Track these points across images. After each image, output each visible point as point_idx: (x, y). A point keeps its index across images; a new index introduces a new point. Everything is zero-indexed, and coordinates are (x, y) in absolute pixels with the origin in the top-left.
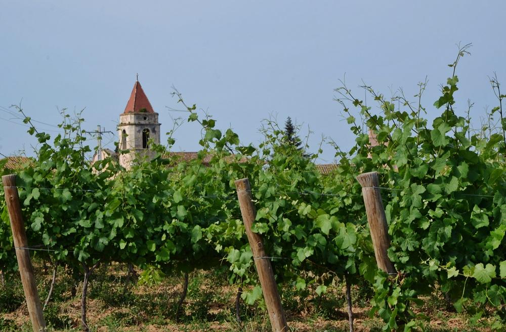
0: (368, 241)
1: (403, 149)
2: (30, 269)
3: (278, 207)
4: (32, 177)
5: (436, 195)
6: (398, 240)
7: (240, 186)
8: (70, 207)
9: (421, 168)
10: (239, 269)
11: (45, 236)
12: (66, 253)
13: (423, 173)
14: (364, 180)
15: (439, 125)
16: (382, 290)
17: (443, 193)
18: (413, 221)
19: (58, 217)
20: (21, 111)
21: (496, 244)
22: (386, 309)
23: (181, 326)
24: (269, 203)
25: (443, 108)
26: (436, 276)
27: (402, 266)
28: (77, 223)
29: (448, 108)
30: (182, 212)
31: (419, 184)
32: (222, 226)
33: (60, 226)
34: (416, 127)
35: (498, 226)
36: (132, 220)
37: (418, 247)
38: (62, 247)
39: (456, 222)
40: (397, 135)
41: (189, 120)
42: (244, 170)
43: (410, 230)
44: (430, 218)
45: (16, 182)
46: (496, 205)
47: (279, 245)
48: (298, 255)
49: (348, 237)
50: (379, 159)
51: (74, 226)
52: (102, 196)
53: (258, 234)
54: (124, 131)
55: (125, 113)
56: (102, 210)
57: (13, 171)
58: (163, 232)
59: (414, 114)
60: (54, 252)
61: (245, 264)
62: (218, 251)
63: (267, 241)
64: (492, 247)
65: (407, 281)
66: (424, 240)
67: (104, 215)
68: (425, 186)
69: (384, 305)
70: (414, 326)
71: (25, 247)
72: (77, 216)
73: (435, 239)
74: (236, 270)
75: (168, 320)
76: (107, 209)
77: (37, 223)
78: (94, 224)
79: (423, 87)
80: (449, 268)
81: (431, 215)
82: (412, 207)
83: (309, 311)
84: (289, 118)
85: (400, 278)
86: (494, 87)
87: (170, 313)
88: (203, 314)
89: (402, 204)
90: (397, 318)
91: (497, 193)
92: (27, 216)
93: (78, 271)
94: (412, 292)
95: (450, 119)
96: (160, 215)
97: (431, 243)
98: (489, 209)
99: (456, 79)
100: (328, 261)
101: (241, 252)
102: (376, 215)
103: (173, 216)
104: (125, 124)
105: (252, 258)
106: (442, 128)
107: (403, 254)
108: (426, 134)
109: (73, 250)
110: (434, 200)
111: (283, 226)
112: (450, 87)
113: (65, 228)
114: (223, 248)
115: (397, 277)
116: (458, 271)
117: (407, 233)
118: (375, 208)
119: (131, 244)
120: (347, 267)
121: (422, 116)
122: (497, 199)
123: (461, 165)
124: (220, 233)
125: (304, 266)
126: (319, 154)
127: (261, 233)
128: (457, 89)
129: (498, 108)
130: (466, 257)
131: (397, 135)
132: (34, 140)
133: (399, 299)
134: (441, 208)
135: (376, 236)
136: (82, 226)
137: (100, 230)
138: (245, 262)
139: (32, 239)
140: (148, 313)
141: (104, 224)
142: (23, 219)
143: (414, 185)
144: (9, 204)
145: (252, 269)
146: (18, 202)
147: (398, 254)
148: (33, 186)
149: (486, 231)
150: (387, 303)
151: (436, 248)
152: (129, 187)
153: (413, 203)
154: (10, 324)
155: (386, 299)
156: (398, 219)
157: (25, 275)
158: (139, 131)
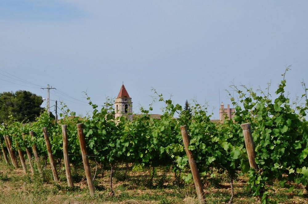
0: (245, 154)
1: (261, 113)
2: (88, 164)
3: (199, 139)
4: (89, 124)
5: (277, 134)
6: (260, 154)
7: (183, 129)
8: (105, 137)
9: (269, 121)
10: (181, 166)
11: (95, 150)
12: (104, 158)
13: (271, 124)
14: (244, 126)
15: (278, 102)
16: (252, 177)
17: (280, 133)
18: (267, 145)
19: (100, 142)
20: (86, 94)
21: (305, 156)
22: (254, 185)
23: (152, 190)
24: (196, 137)
25: (280, 94)
26: (277, 171)
27: (262, 166)
28: (108, 145)
29: (281, 94)
30: (155, 142)
31: (269, 129)
32: (173, 146)
33: (101, 146)
34: (267, 103)
35: (305, 148)
36: (132, 144)
37: (269, 157)
38: (102, 155)
39: (287, 146)
40: (258, 106)
41: (159, 100)
42: (184, 122)
43: (265, 150)
44: (274, 144)
45: (82, 127)
46: (304, 138)
47: (200, 156)
48: (209, 160)
49: (236, 152)
50: (245, 117)
51: (107, 146)
52: (119, 133)
53: (191, 150)
54: (117, 106)
55: (118, 98)
56: (119, 139)
57: (81, 122)
58: (146, 149)
59: (265, 97)
60: (98, 157)
61: (184, 164)
62: (172, 158)
63: (195, 154)
64: (303, 158)
65: (264, 173)
66: (272, 154)
67: (120, 141)
68: (272, 130)
69: (253, 184)
70: (268, 194)
71: (86, 155)
72: (108, 142)
73: (277, 154)
74: (180, 166)
75: (146, 188)
76: (122, 138)
77: (92, 144)
78: (116, 145)
79: (269, 85)
80: (290, 169)
81: (275, 143)
82: (266, 139)
83: (207, 184)
84: (187, 100)
85: (261, 172)
86: (303, 85)
87: (147, 185)
88: (161, 185)
89: (261, 138)
90: (260, 190)
91: (305, 133)
92: (87, 141)
93: (106, 166)
94: (267, 178)
95: (283, 99)
96: (144, 142)
97: (275, 156)
98: (301, 140)
99: (285, 81)
100: (223, 162)
101: (183, 158)
102: (250, 143)
103: (152, 143)
104: (118, 103)
105: (188, 161)
106: (279, 103)
107: (262, 161)
108: (271, 106)
109: (107, 157)
110: (276, 136)
111: (202, 147)
112: (282, 85)
113: (103, 147)
114: (175, 156)
115: (259, 171)
116: (294, 170)
117: (264, 151)
118: (249, 140)
119: (132, 154)
120: (231, 166)
121: (269, 98)
122: (305, 136)
123: (288, 120)
124: (172, 150)
125: (211, 165)
126: (212, 115)
127: (192, 150)
128: (286, 86)
129: (305, 95)
130: (291, 162)
131: (258, 106)
132: (91, 107)
133: (261, 181)
134: (280, 140)
135: (250, 152)
136: (111, 146)
137: (118, 148)
138: (184, 163)
139: (89, 152)
140: (137, 184)
141: (121, 145)
142: (85, 142)
143: (267, 129)
144: (79, 136)
145: (187, 166)
146: (83, 135)
147: (260, 160)
148: (90, 128)
149: (300, 151)
150: (255, 183)
151: (277, 158)
152: (131, 128)
153: (266, 137)
154: (78, 188)
155: (255, 181)
156: (260, 144)
157: (86, 167)
158: (123, 106)
